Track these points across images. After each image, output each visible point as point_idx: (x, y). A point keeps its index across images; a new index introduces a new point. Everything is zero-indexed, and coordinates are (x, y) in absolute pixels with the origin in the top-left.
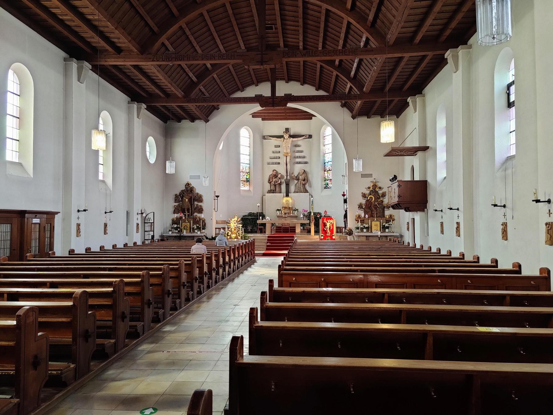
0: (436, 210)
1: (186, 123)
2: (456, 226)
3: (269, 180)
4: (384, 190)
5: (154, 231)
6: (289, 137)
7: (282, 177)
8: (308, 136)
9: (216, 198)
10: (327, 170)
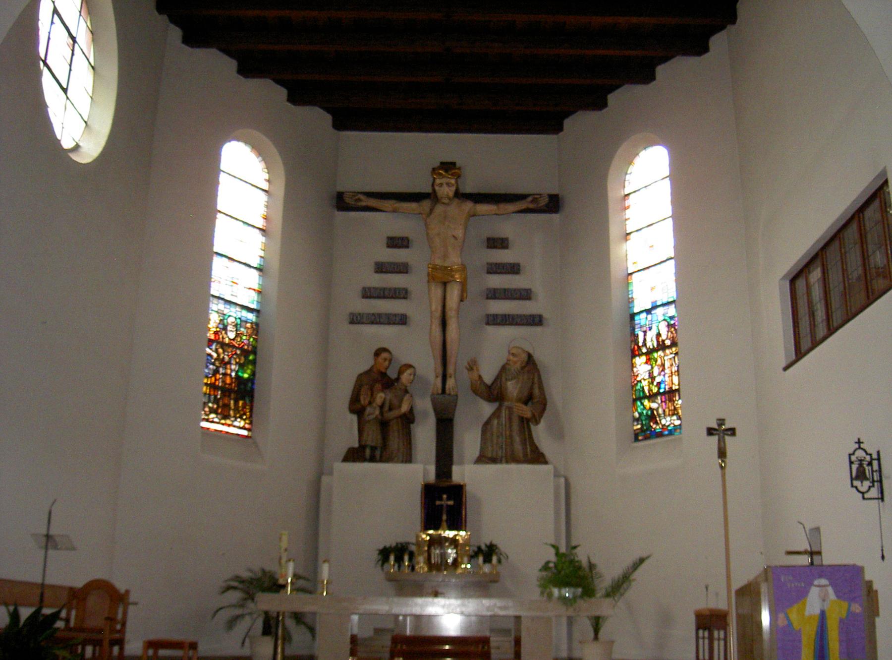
10: (649, 344)
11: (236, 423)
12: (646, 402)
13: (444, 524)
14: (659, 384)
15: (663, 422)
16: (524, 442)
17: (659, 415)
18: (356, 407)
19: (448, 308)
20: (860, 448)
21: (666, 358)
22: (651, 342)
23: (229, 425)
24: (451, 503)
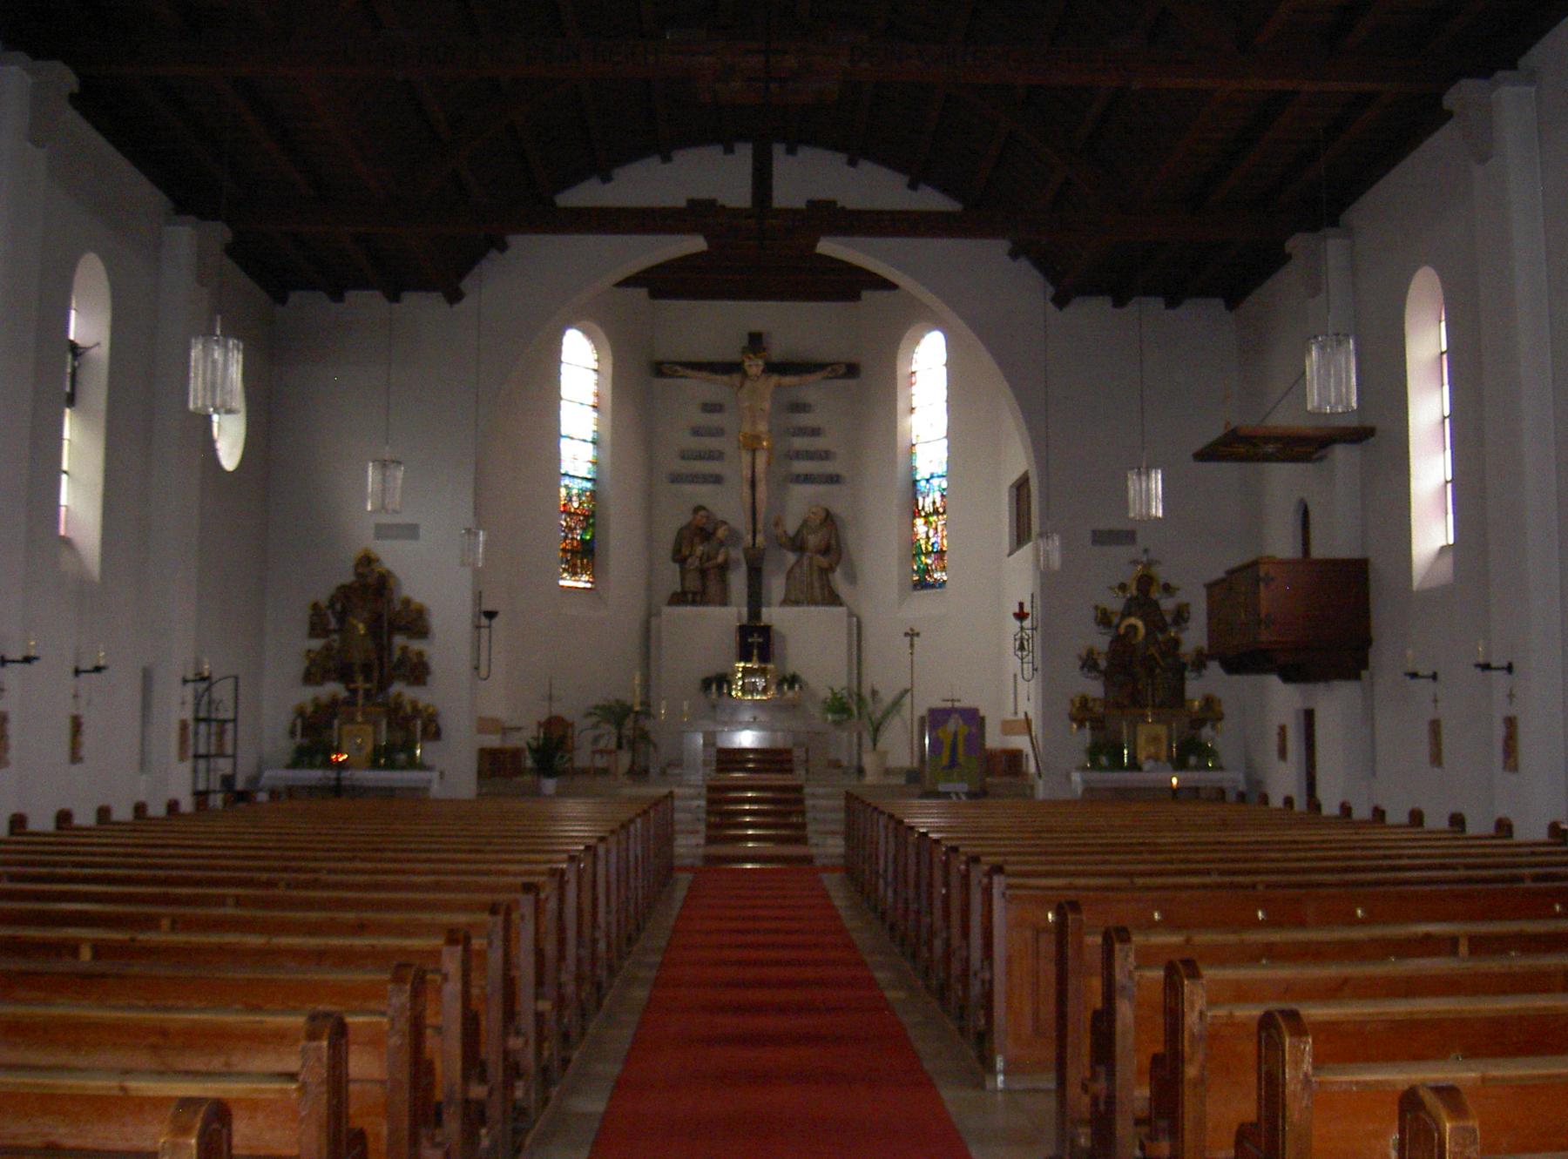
0: (1414, 675)
1: (366, 304)
2: (1500, 731)
4: (1181, 597)
5: (234, 756)
6: (763, 371)
7: (734, 536)
8: (842, 370)
9: (484, 621)
10: (927, 509)
11: (583, 579)
13: (755, 658)
15: (935, 576)
16: (822, 588)
17: (932, 570)
18: (679, 557)
19: (757, 500)
21: (939, 523)
22: (929, 508)
23: (578, 581)
24: (761, 640)
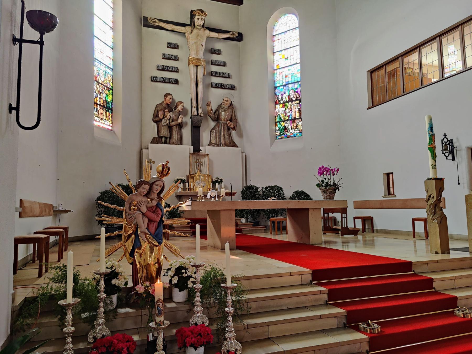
3: (156, 115)
7: (184, 112)
10: (284, 99)
11: (106, 123)
12: (282, 123)
14: (289, 116)
18: (157, 120)
20: (445, 137)
